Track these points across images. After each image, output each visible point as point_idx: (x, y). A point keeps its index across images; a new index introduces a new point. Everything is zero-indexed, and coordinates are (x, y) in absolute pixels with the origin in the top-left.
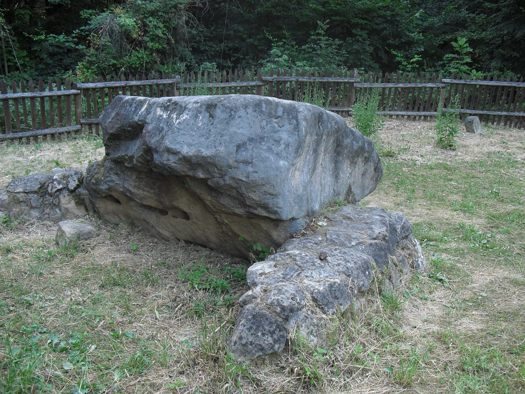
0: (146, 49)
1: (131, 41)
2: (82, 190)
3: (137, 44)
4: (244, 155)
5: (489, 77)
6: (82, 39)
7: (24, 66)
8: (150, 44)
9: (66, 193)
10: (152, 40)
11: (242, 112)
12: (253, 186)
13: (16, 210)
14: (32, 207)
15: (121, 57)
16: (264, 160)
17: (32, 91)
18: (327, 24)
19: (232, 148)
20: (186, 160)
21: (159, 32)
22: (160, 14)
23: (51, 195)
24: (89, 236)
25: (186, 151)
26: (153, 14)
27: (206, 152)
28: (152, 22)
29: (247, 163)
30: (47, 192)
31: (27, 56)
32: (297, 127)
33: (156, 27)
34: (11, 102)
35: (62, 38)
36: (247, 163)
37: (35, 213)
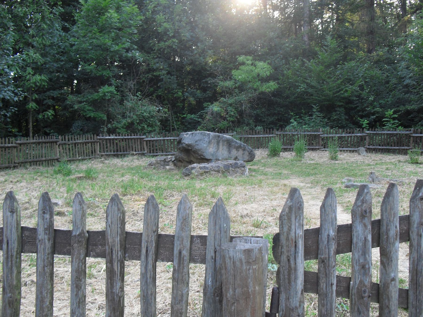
0: (227, 120)
1: (221, 117)
2: (175, 161)
3: (225, 119)
4: (197, 143)
5: (351, 132)
6: (201, 117)
7: (178, 128)
8: (228, 119)
9: (171, 162)
10: (230, 117)
11: (198, 134)
12: (199, 150)
13: (157, 165)
14: (162, 165)
15: (216, 125)
16: (201, 144)
17: (174, 137)
18: (318, 106)
19: (195, 142)
20: (186, 145)
21: (232, 113)
22: (233, 105)
23: (167, 162)
24: (173, 169)
25: (187, 143)
26: (231, 105)
27: (190, 143)
28: (230, 108)
29: (198, 145)
30: (166, 161)
31: (180, 124)
32: (209, 138)
33: (231, 111)
34: (166, 141)
35: (193, 116)
36: (198, 145)
37: (162, 167)
